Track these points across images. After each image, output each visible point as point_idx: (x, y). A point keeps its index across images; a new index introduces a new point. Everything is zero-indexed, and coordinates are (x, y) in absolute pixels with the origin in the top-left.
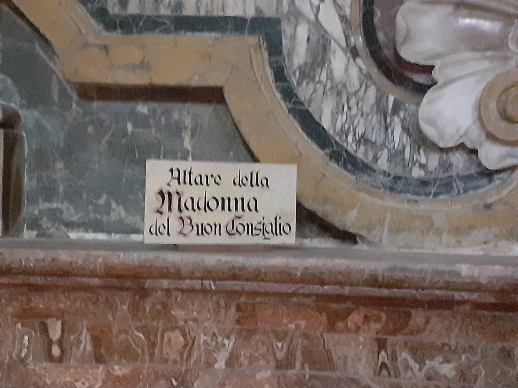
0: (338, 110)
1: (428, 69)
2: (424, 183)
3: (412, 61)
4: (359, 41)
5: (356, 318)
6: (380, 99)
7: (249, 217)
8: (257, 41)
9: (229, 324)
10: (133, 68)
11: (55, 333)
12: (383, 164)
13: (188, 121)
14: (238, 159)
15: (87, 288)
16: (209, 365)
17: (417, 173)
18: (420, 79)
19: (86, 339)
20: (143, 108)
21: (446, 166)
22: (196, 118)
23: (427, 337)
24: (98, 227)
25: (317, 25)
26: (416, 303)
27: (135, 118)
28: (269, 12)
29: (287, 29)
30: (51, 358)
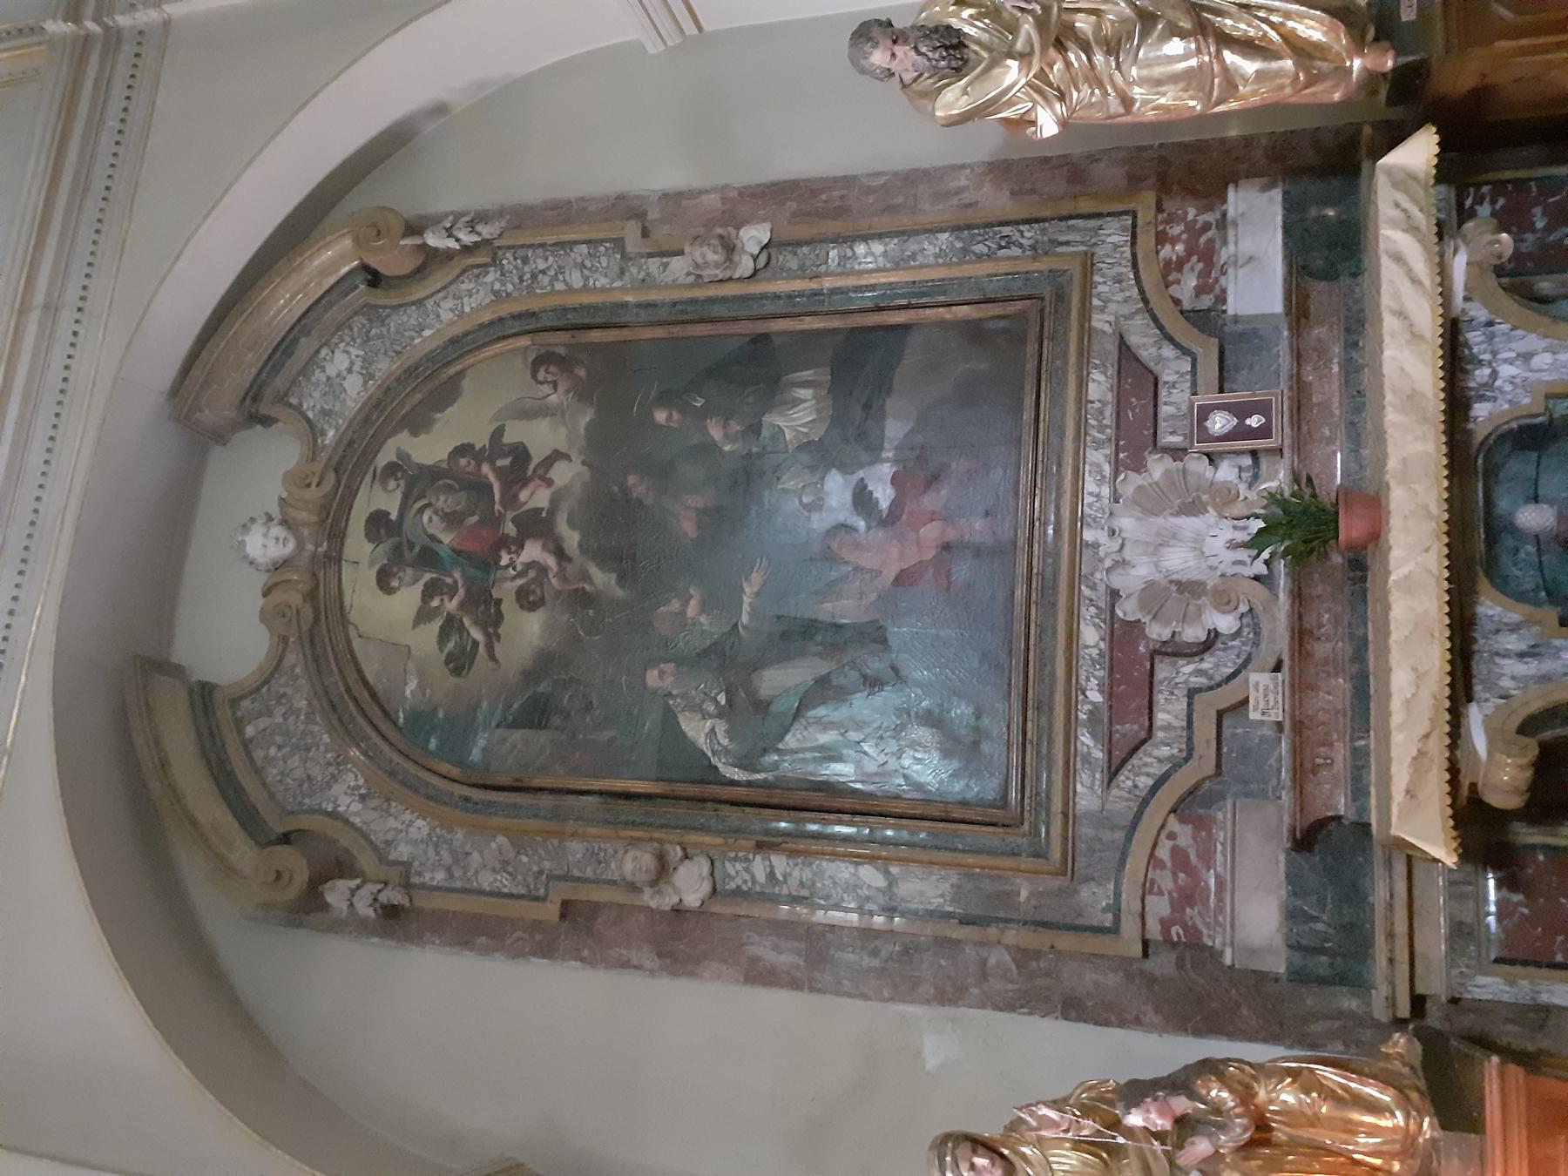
0: (1226, 666)
1: (1209, 631)
2: (1255, 633)
3: (1165, 1074)
4: (1197, 659)
5: (1309, 647)
6: (1219, 649)
7: (1271, 687)
8: (1240, 243)
9: (1313, 694)
10: (1208, 747)
11: (1321, 761)
12: (1248, 648)
13: (1231, 730)
14: (1247, 709)
15: (1301, 743)
16: (1330, 702)
17: (1251, 636)
18: (1212, 635)
19: (1323, 749)
20: (1225, 749)
21: (1248, 625)
22: (1229, 727)
23: (1314, 623)
24: (1279, 771)
25: (1190, 674)
26: (1301, 625)
27: (1231, 750)
28: (1185, 692)
29: (1192, 686)
30: (1332, 764)
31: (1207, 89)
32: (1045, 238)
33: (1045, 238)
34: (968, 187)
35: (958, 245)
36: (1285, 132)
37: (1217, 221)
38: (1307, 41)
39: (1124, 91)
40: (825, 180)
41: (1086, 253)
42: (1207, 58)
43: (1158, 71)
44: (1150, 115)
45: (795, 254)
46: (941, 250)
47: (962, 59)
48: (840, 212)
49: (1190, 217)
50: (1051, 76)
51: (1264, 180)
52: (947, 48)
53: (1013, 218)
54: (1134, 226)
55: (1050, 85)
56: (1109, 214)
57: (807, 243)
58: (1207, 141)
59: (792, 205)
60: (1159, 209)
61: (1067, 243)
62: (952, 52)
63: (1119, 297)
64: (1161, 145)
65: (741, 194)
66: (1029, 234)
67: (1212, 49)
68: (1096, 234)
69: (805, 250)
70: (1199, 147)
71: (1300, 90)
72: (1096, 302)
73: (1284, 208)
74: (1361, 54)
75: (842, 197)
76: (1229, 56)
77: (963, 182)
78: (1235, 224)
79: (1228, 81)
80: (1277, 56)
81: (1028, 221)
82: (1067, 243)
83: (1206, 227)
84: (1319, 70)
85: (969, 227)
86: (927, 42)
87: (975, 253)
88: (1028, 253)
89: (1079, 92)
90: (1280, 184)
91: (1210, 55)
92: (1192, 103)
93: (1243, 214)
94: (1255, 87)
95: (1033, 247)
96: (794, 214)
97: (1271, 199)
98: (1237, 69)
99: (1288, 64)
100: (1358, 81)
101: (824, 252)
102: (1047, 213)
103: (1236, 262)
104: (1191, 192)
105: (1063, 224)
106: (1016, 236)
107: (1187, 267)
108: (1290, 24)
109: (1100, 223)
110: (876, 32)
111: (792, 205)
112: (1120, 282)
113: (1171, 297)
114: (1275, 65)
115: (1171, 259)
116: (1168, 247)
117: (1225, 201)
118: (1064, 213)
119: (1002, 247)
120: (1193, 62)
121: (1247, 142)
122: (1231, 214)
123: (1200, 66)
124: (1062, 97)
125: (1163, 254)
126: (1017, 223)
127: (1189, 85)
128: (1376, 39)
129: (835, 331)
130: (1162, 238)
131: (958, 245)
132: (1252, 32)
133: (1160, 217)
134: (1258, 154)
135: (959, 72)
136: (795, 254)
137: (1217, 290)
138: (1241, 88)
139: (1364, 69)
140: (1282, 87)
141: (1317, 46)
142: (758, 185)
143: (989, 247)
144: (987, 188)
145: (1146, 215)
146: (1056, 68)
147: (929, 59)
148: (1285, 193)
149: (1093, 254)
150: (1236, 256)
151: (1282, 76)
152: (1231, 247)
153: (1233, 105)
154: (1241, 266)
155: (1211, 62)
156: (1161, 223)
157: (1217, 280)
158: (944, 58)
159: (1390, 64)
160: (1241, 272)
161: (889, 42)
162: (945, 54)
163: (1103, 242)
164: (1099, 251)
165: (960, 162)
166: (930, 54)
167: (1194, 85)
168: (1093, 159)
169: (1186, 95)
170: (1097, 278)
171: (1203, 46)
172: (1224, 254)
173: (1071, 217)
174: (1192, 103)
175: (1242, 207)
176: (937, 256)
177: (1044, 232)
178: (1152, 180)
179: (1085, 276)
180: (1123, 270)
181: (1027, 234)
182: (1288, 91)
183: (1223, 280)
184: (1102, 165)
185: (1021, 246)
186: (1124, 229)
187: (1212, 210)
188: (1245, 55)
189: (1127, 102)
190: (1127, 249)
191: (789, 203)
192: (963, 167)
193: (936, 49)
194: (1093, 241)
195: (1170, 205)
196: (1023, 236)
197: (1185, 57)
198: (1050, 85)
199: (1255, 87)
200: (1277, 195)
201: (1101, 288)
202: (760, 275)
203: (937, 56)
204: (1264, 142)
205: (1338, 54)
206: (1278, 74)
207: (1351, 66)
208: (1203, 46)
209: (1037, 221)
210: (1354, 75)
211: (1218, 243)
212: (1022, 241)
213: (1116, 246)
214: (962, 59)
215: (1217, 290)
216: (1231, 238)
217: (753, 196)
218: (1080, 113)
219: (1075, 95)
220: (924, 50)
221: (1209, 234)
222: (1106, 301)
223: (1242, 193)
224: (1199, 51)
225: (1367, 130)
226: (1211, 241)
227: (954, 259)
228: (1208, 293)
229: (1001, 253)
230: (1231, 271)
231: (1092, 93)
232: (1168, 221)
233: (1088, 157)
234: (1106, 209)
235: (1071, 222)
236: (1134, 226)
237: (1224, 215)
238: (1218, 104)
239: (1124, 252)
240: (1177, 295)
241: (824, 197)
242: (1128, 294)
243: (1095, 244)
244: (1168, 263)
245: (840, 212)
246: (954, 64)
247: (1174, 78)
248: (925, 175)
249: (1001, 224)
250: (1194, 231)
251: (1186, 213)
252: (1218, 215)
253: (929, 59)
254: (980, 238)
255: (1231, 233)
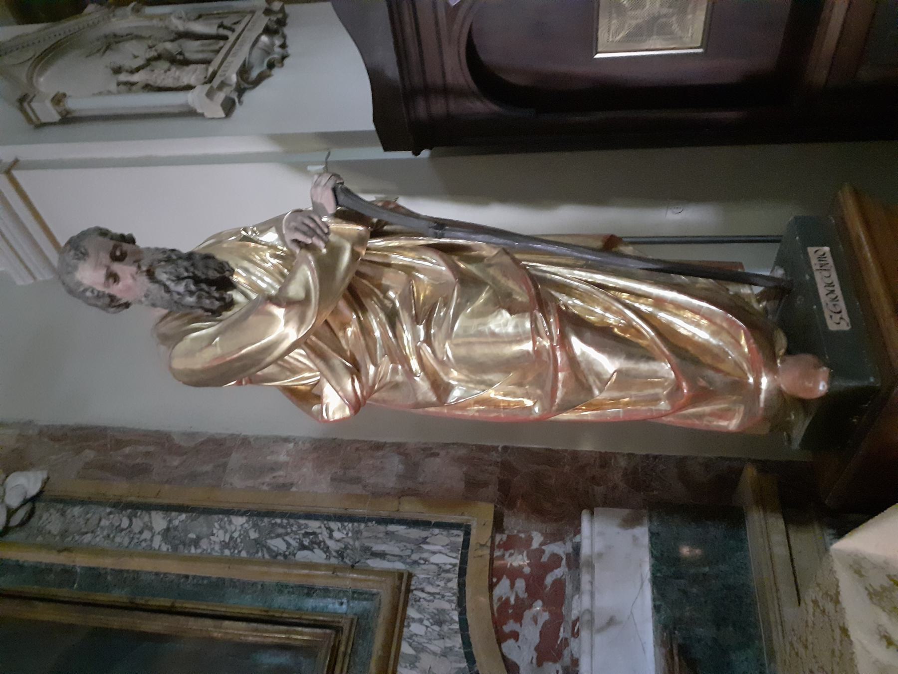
31: (548, 387)
32: (357, 544)
33: (357, 544)
34: (288, 463)
35: (253, 535)
36: (647, 456)
37: (568, 555)
38: (688, 339)
39: (435, 373)
40: (124, 431)
41: (401, 575)
42: (547, 343)
43: (481, 351)
44: (474, 411)
45: (63, 514)
46: (231, 538)
47: (221, 299)
48: (138, 471)
49: (535, 545)
50: (343, 342)
51: (625, 512)
52: (197, 280)
53: (325, 511)
54: (466, 544)
55: (340, 352)
56: (439, 525)
57: (82, 502)
58: (558, 452)
59: (89, 455)
60: (498, 525)
61: (382, 555)
62: (204, 286)
63: (437, 646)
64: (505, 448)
65: (41, 433)
66: (341, 532)
67: (556, 332)
68: (420, 549)
69: (77, 510)
70: (550, 457)
71: (684, 407)
72: (406, 648)
73: (653, 556)
74: (772, 369)
75: (147, 454)
76: (578, 346)
77: (283, 458)
78: (590, 566)
79: (577, 379)
80: (648, 356)
81: (340, 518)
82: (382, 555)
83: (555, 560)
84: (710, 383)
85: (270, 514)
86: (170, 268)
87: (269, 549)
88: (334, 561)
89: (376, 365)
90: (646, 520)
91: (551, 338)
92: (529, 403)
93: (600, 555)
94: (615, 394)
95: (341, 554)
96: (88, 466)
97: (635, 539)
98: (590, 363)
99: (665, 368)
100: (767, 407)
101: (97, 516)
102: (361, 510)
103: (591, 622)
104: (538, 512)
105: (382, 528)
106: (324, 535)
107: (528, 615)
108: (663, 316)
109: (424, 534)
110: (89, 245)
111: (89, 455)
112: (440, 623)
113: (504, 658)
114: (644, 367)
115: (508, 599)
116: (505, 582)
117: (578, 531)
118: (384, 514)
119: (303, 547)
120: (528, 346)
121: (604, 460)
122: (585, 550)
123: (538, 352)
124: (356, 370)
125: (499, 591)
126: (329, 518)
127: (524, 377)
128: (789, 352)
129: (70, 628)
130: (495, 574)
131: (253, 535)
132: (611, 319)
133: (498, 538)
134: (617, 477)
135: (214, 314)
136: (63, 514)
137: (567, 660)
138: (597, 392)
139: (778, 394)
140: (656, 399)
141: (704, 347)
142: (63, 426)
143: (289, 545)
144: (307, 469)
145: (481, 534)
146: (349, 331)
147: (167, 290)
148: (653, 535)
149: (410, 576)
150: (590, 612)
151: (654, 385)
152: (586, 599)
153: (588, 415)
154: (601, 630)
155: (553, 348)
156: (499, 546)
157: (566, 642)
158: (191, 293)
159: (822, 387)
160: (598, 638)
161: (105, 258)
162: (193, 288)
163: (426, 560)
164: (420, 574)
165: (284, 433)
166: (172, 285)
167: (530, 379)
168: (429, 452)
169: (519, 391)
170: (412, 612)
171: (542, 324)
172: (578, 606)
173: (392, 521)
174: (529, 403)
175: (599, 546)
176: (225, 545)
177: (357, 533)
178: (492, 490)
179: (395, 609)
180: (446, 606)
181: (337, 535)
182: (664, 405)
183: (573, 644)
184: (438, 460)
185: (326, 549)
186: (452, 547)
187: (563, 539)
188: (600, 348)
189: (441, 388)
190: (454, 576)
191: (87, 451)
192: (286, 440)
193: (179, 279)
194: (415, 557)
195: (514, 523)
196: (331, 537)
197: (518, 339)
198: (340, 352)
199: (615, 394)
200: (642, 533)
201: (415, 628)
202: (12, 537)
203: (181, 288)
204: (623, 463)
205: (738, 365)
206: (647, 380)
207: (758, 383)
208: (542, 324)
209: (352, 519)
210: (762, 396)
211: (569, 589)
212: (330, 543)
213: (441, 570)
214: (221, 299)
215: (567, 660)
216: (585, 586)
217: (55, 439)
218: (383, 395)
219: (372, 369)
220: (163, 277)
221: (558, 573)
222: (420, 649)
223: (597, 526)
224: (535, 331)
225: (750, 472)
226: (559, 584)
227: (244, 554)
228: (555, 661)
229: (302, 555)
230: (585, 634)
231: (394, 370)
232: (508, 546)
233: (424, 450)
234: (434, 517)
235: (392, 528)
236: (466, 544)
237: (577, 549)
238: (564, 408)
239: (449, 580)
240: (513, 656)
241: (127, 450)
242: (449, 643)
243: (416, 563)
244: (505, 603)
245: (138, 471)
246: (207, 302)
247: (506, 365)
248: (245, 442)
249: (309, 516)
250: (541, 568)
251: (530, 540)
252: (569, 548)
253: (167, 290)
254: (280, 531)
255: (585, 578)
